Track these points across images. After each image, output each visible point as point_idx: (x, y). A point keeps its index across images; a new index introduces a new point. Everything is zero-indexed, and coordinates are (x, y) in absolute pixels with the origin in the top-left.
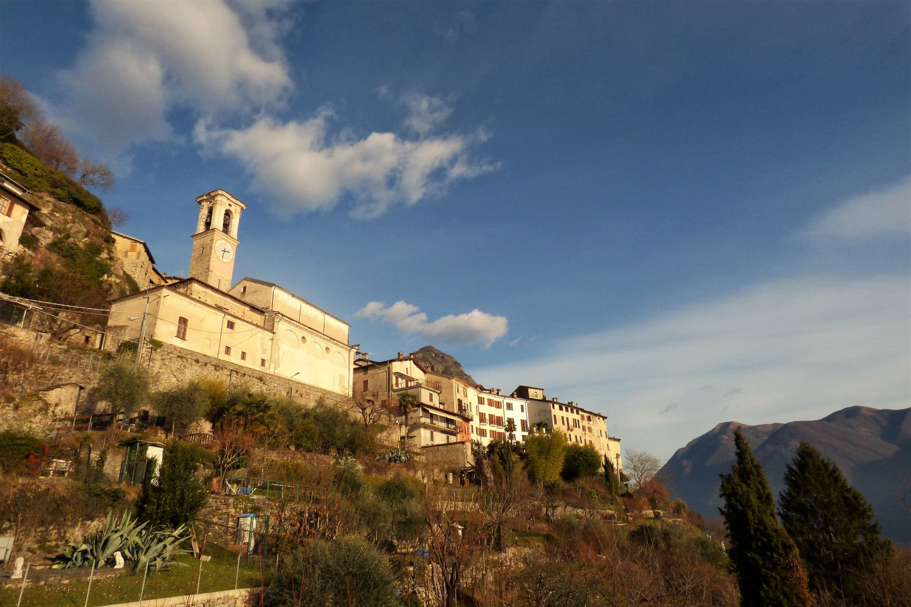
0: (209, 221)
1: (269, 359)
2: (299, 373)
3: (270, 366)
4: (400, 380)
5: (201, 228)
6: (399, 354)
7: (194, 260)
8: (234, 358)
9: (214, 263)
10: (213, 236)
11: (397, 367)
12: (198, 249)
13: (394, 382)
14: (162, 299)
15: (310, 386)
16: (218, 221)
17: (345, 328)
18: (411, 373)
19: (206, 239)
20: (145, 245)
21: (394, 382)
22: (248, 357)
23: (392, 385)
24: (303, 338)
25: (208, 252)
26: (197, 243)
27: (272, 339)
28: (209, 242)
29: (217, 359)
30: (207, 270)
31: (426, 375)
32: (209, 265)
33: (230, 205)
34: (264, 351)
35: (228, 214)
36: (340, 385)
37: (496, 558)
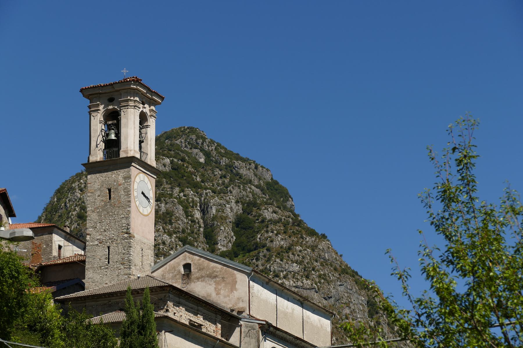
0: (113, 137)
12: (99, 189)
25: (123, 199)
28: (121, 179)
30: (126, 235)
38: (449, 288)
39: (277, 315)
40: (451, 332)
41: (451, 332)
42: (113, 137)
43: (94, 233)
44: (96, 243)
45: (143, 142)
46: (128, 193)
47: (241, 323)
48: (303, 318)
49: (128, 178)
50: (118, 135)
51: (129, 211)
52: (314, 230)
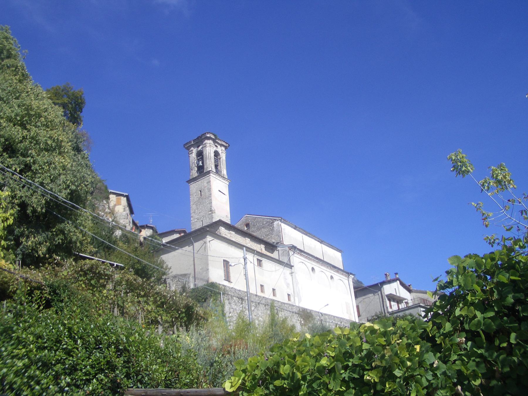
0: (201, 164)
1: (293, 294)
2: (328, 305)
3: (295, 300)
4: (392, 303)
5: (194, 173)
6: (386, 275)
7: (193, 204)
8: (268, 294)
9: (215, 204)
10: (210, 178)
11: (388, 289)
12: (196, 192)
13: (388, 305)
14: (208, 244)
15: (334, 317)
16: (210, 165)
17: (338, 255)
18: (399, 293)
19: (202, 183)
20: (127, 197)
21: (388, 305)
22: (277, 292)
23: (387, 308)
24: (313, 269)
25: (207, 194)
26: (194, 187)
27: (292, 273)
28: (205, 184)
29: (256, 295)
30: (210, 212)
31: (412, 294)
32: (211, 206)
33: (216, 146)
34: (288, 285)
35: (216, 154)
36: (347, 313)
37: (38, 372)
38: (199, 310)
39: (194, 260)
40: (165, 240)
41: (165, 240)
42: (201, 164)
43: (195, 215)
44: (196, 220)
45: (218, 166)
46: (210, 190)
47: (279, 248)
48: (195, 276)
49: (209, 182)
50: (203, 163)
51: (211, 199)
52: (391, 294)
